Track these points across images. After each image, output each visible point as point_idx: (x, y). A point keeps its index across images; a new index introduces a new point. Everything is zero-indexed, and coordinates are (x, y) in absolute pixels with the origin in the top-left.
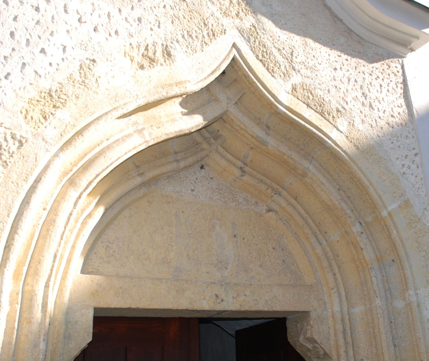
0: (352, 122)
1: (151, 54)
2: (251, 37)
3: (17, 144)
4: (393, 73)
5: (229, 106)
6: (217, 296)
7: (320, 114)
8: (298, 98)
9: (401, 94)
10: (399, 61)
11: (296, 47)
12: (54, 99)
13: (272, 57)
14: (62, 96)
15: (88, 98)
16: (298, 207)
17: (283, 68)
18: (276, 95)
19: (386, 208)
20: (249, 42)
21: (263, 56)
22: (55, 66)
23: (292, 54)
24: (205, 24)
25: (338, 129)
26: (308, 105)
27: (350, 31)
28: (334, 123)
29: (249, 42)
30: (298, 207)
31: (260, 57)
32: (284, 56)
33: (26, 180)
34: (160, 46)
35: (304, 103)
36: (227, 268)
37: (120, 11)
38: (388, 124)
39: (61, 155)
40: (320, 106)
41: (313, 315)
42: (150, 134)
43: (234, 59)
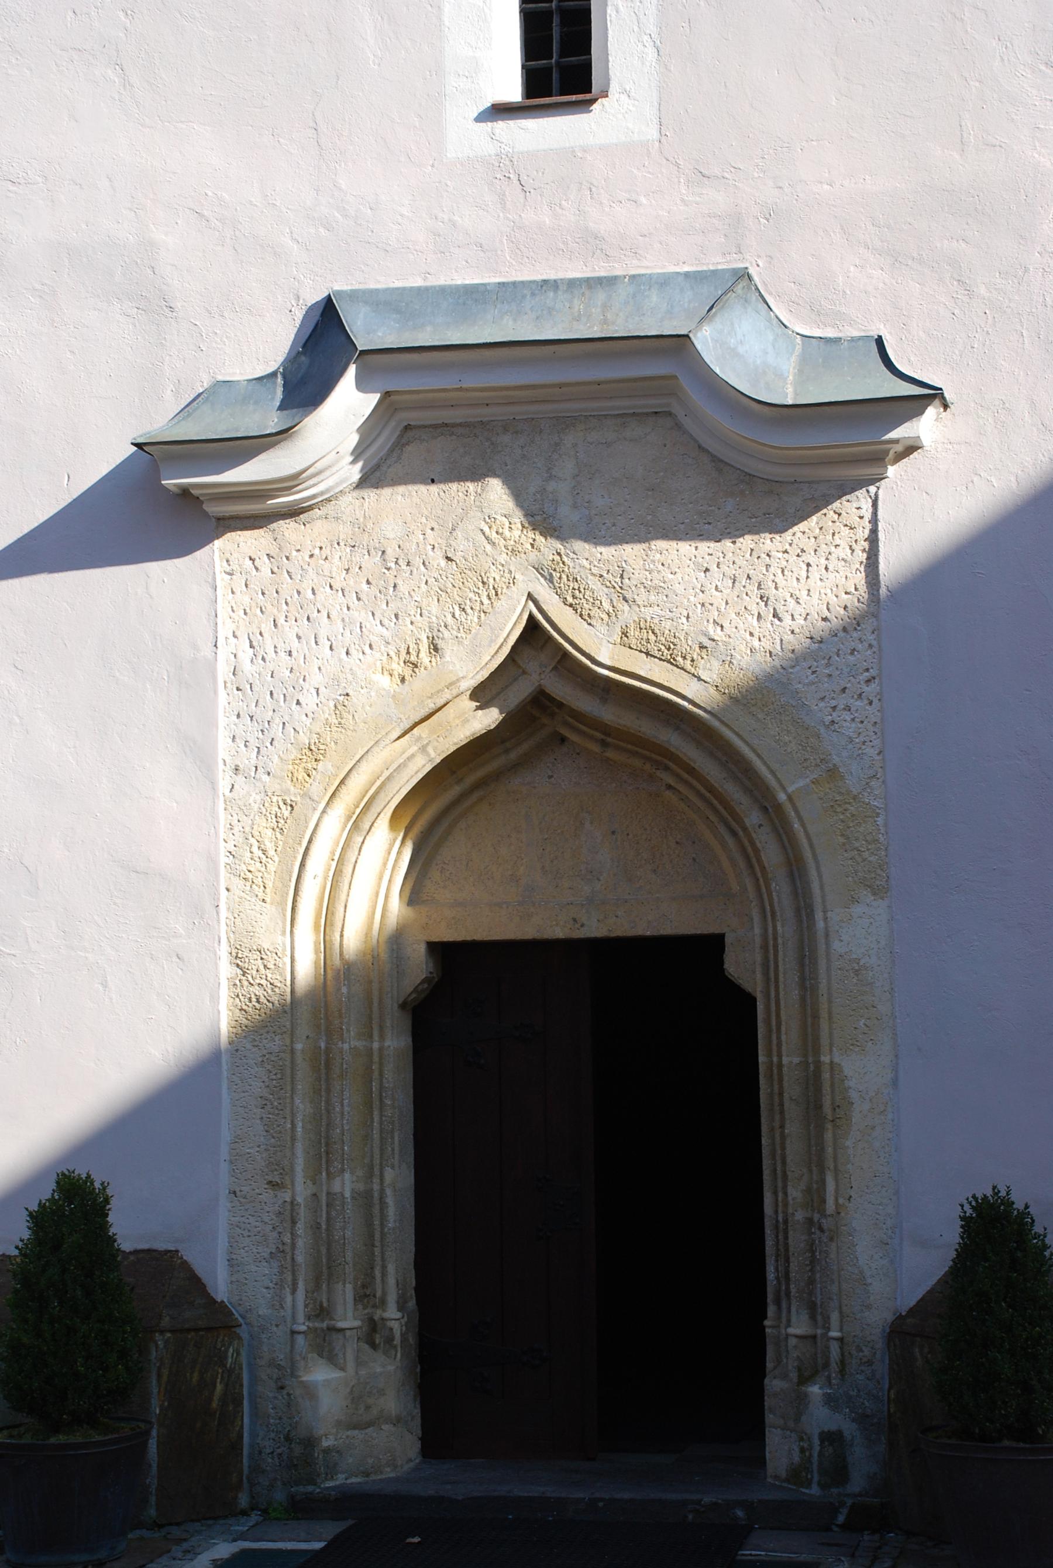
0: (729, 658)
1: (413, 658)
2: (554, 574)
3: (289, 808)
4: (846, 525)
5: (543, 676)
6: (575, 920)
7: (669, 662)
8: (630, 648)
9: (861, 563)
10: (868, 491)
11: (631, 561)
12: (314, 751)
13: (588, 593)
14: (322, 747)
15: (347, 740)
16: (695, 783)
17: (606, 605)
18: (593, 654)
19: (784, 789)
20: (552, 583)
21: (574, 597)
22: (310, 715)
23: (622, 577)
24: (483, 583)
25: (699, 679)
26: (647, 654)
27: (749, 478)
28: (693, 671)
29: (552, 583)
30: (695, 783)
31: (570, 600)
32: (608, 584)
33: (300, 844)
34: (425, 640)
35: (641, 651)
36: (599, 880)
37: (373, 614)
38: (811, 638)
39: (329, 810)
40: (669, 649)
41: (728, 940)
42: (435, 749)
43: (531, 618)
